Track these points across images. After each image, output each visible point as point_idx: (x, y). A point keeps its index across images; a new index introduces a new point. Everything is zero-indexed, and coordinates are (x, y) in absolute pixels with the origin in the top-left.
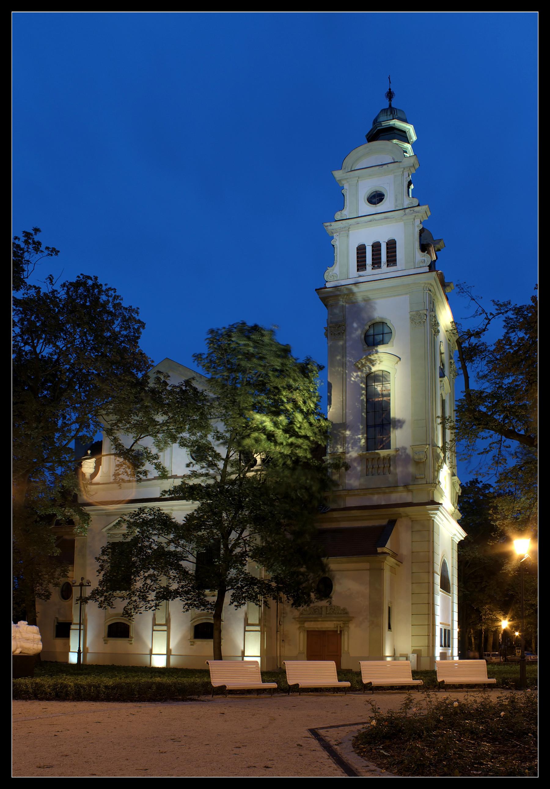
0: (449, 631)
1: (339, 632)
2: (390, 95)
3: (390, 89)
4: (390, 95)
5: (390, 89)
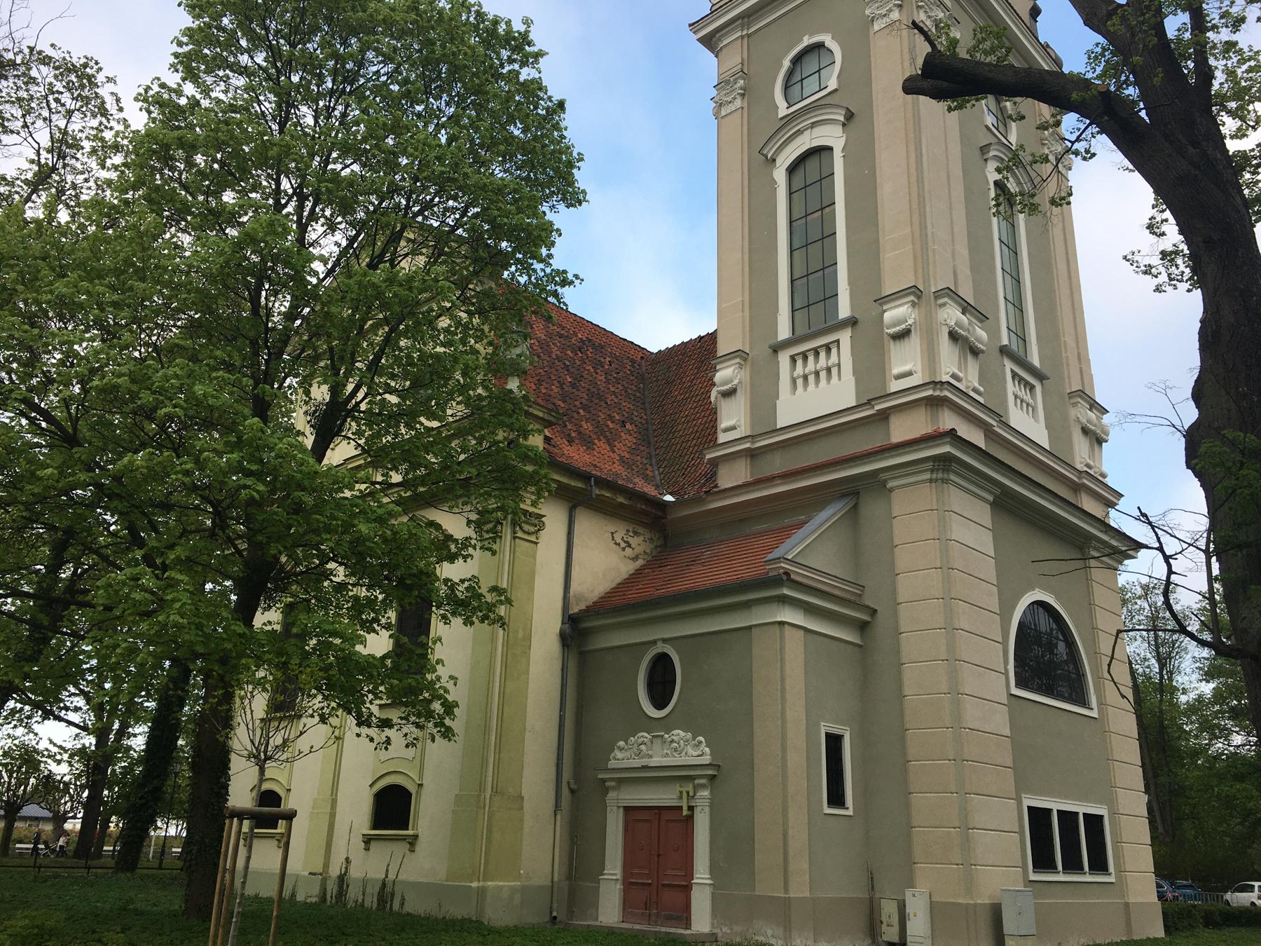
0: (1094, 822)
1: (685, 812)
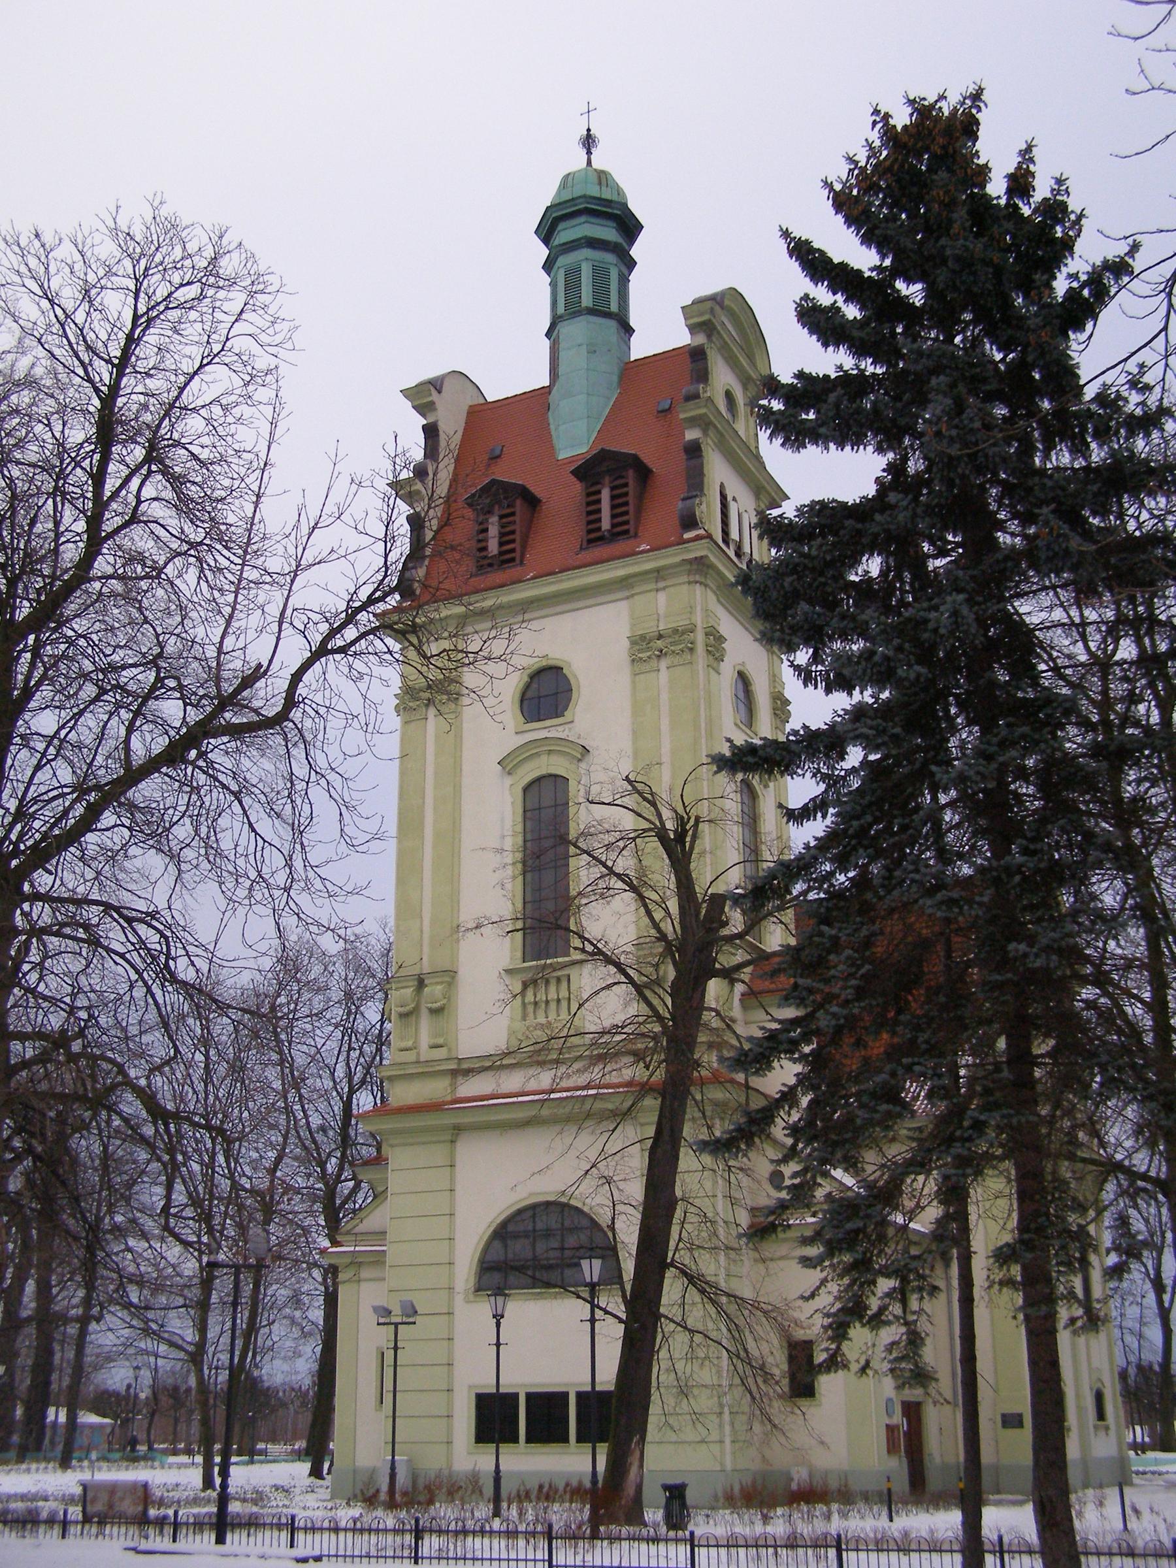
2: (589, 141)
3: (589, 130)
4: (589, 141)
5: (589, 130)
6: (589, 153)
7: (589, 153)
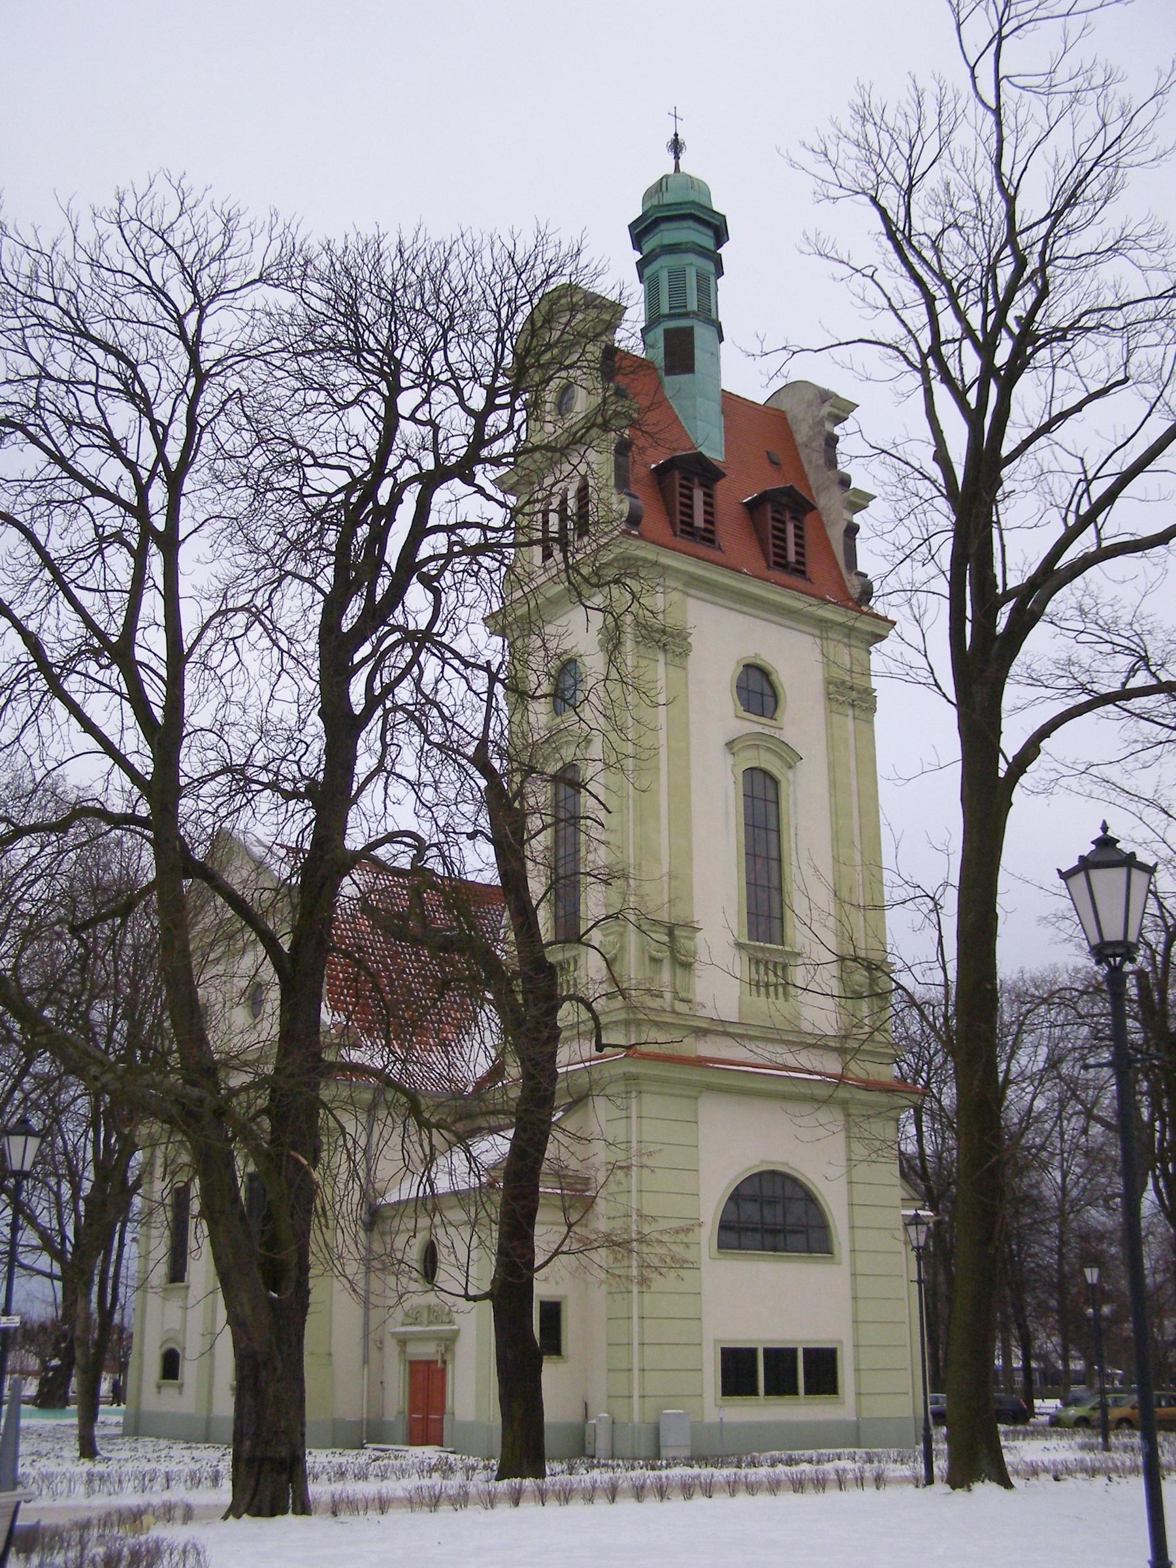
2: (676, 146)
4: (676, 146)
6: (677, 158)
7: (677, 158)
